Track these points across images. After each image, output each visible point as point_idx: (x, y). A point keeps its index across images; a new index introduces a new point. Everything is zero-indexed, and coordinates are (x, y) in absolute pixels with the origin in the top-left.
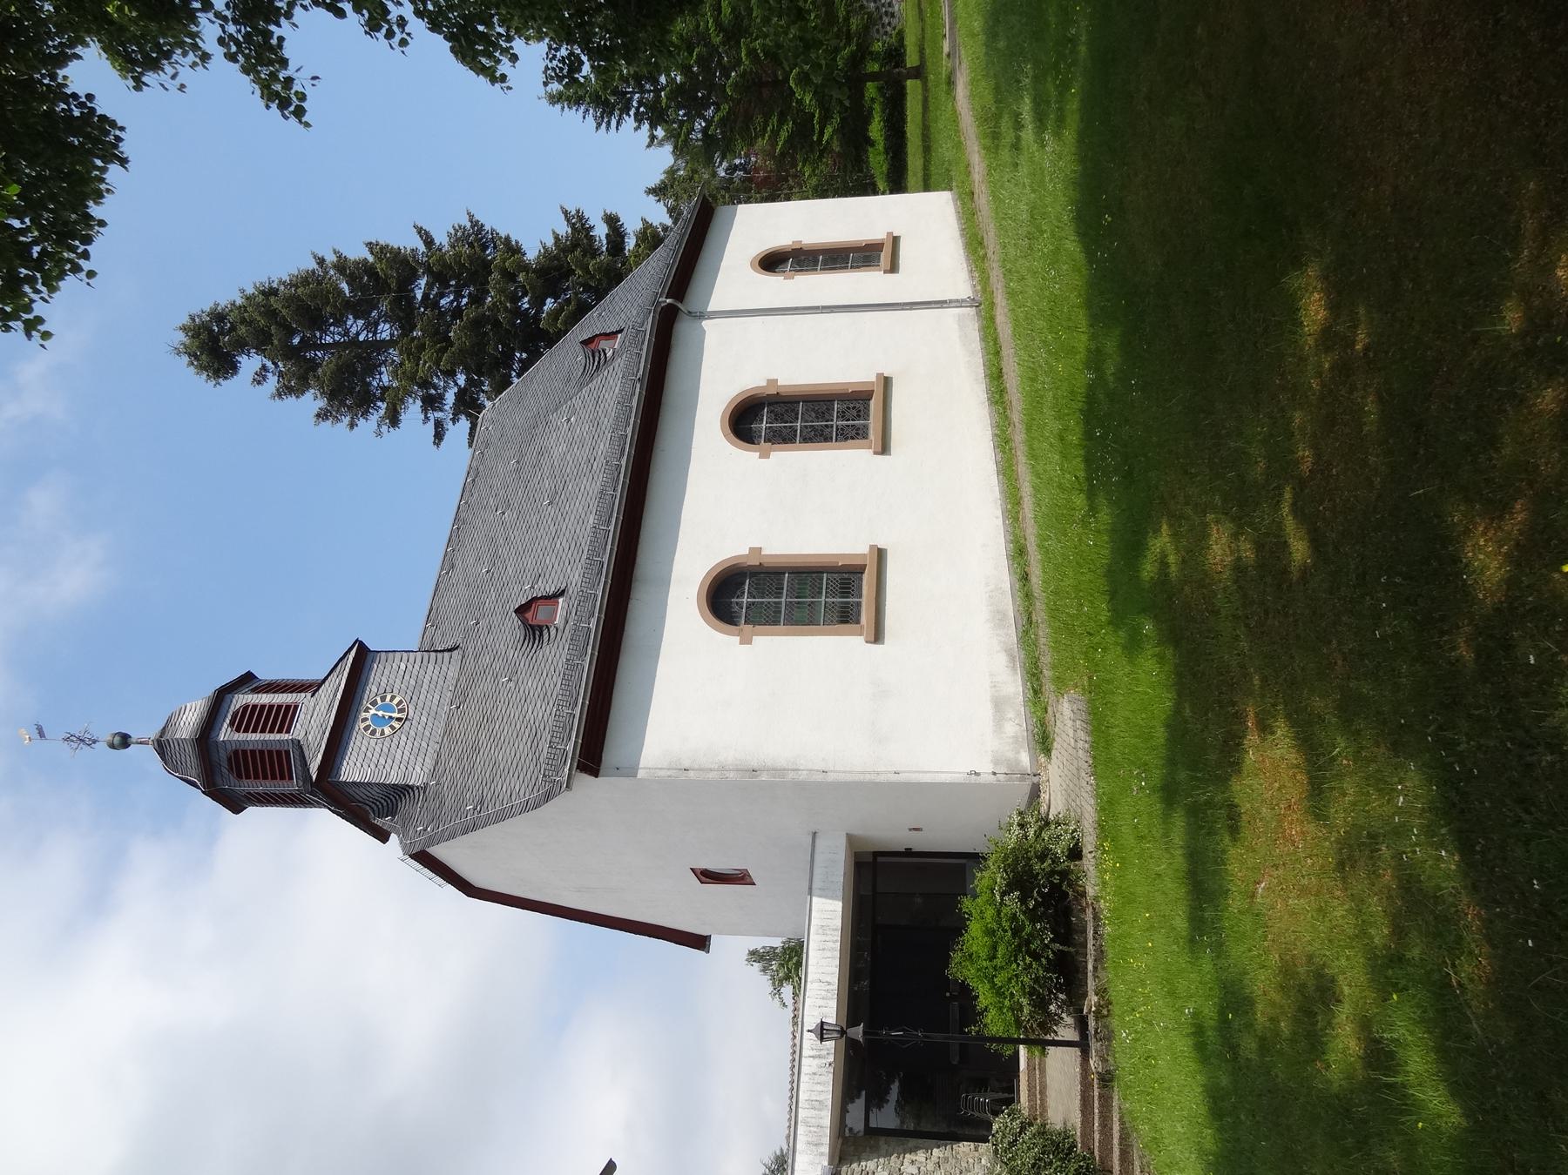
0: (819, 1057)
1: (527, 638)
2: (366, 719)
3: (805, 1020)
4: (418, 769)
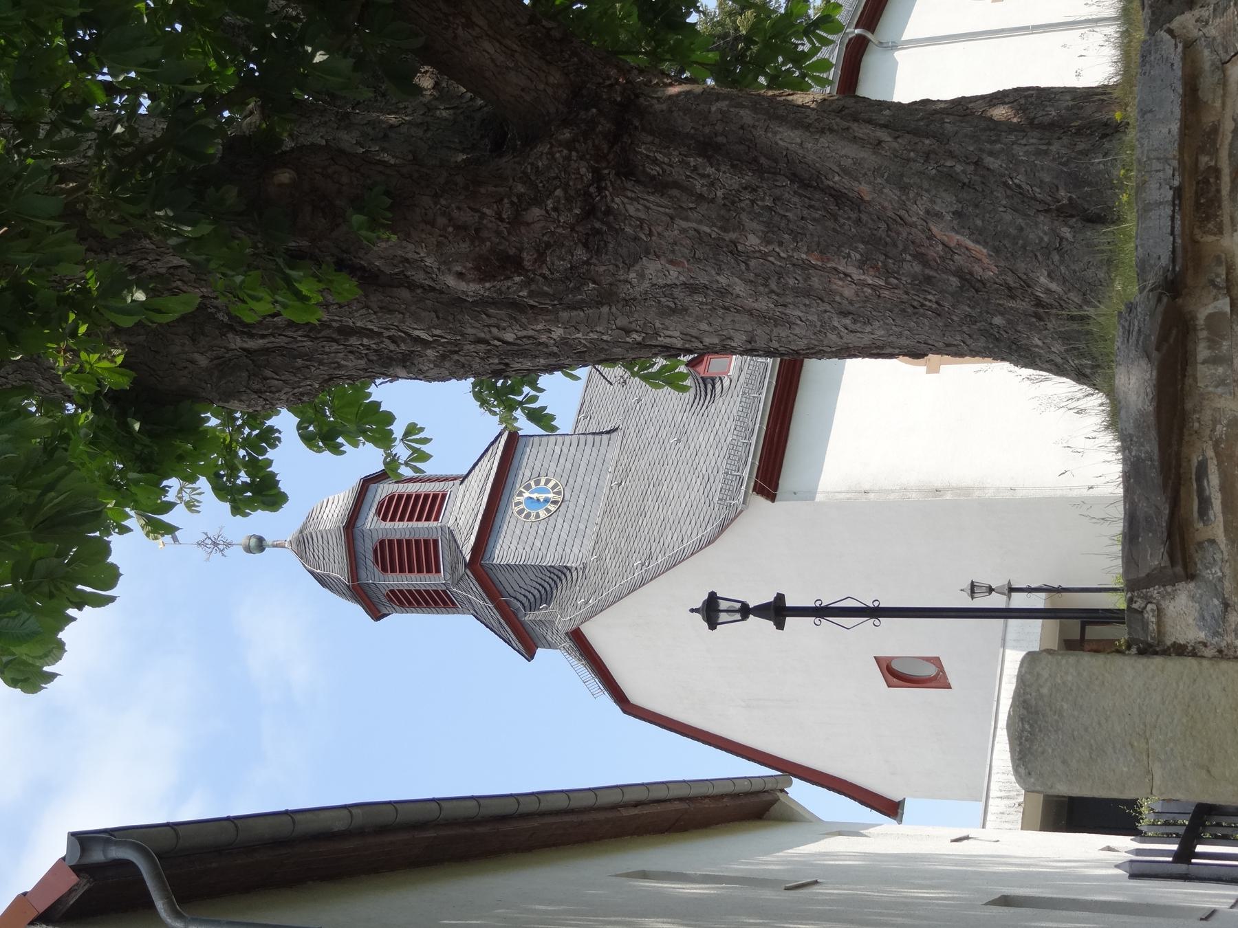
0: (1008, 797)
1: (698, 399)
2: (520, 503)
3: (993, 764)
4: (576, 550)
